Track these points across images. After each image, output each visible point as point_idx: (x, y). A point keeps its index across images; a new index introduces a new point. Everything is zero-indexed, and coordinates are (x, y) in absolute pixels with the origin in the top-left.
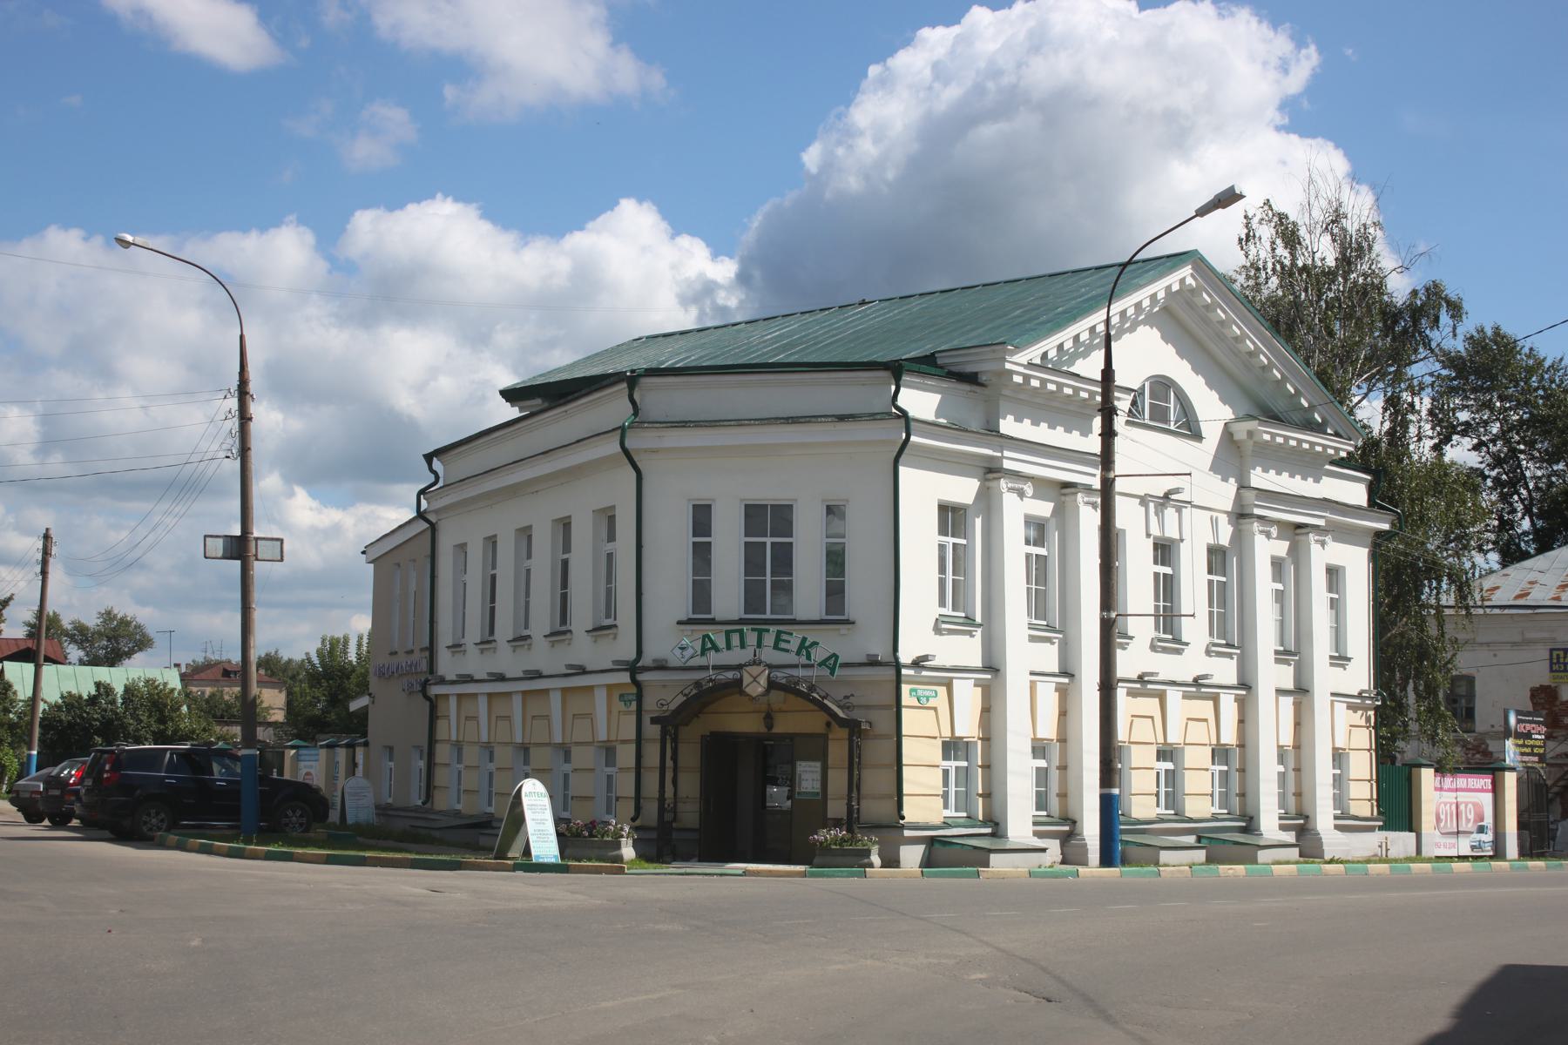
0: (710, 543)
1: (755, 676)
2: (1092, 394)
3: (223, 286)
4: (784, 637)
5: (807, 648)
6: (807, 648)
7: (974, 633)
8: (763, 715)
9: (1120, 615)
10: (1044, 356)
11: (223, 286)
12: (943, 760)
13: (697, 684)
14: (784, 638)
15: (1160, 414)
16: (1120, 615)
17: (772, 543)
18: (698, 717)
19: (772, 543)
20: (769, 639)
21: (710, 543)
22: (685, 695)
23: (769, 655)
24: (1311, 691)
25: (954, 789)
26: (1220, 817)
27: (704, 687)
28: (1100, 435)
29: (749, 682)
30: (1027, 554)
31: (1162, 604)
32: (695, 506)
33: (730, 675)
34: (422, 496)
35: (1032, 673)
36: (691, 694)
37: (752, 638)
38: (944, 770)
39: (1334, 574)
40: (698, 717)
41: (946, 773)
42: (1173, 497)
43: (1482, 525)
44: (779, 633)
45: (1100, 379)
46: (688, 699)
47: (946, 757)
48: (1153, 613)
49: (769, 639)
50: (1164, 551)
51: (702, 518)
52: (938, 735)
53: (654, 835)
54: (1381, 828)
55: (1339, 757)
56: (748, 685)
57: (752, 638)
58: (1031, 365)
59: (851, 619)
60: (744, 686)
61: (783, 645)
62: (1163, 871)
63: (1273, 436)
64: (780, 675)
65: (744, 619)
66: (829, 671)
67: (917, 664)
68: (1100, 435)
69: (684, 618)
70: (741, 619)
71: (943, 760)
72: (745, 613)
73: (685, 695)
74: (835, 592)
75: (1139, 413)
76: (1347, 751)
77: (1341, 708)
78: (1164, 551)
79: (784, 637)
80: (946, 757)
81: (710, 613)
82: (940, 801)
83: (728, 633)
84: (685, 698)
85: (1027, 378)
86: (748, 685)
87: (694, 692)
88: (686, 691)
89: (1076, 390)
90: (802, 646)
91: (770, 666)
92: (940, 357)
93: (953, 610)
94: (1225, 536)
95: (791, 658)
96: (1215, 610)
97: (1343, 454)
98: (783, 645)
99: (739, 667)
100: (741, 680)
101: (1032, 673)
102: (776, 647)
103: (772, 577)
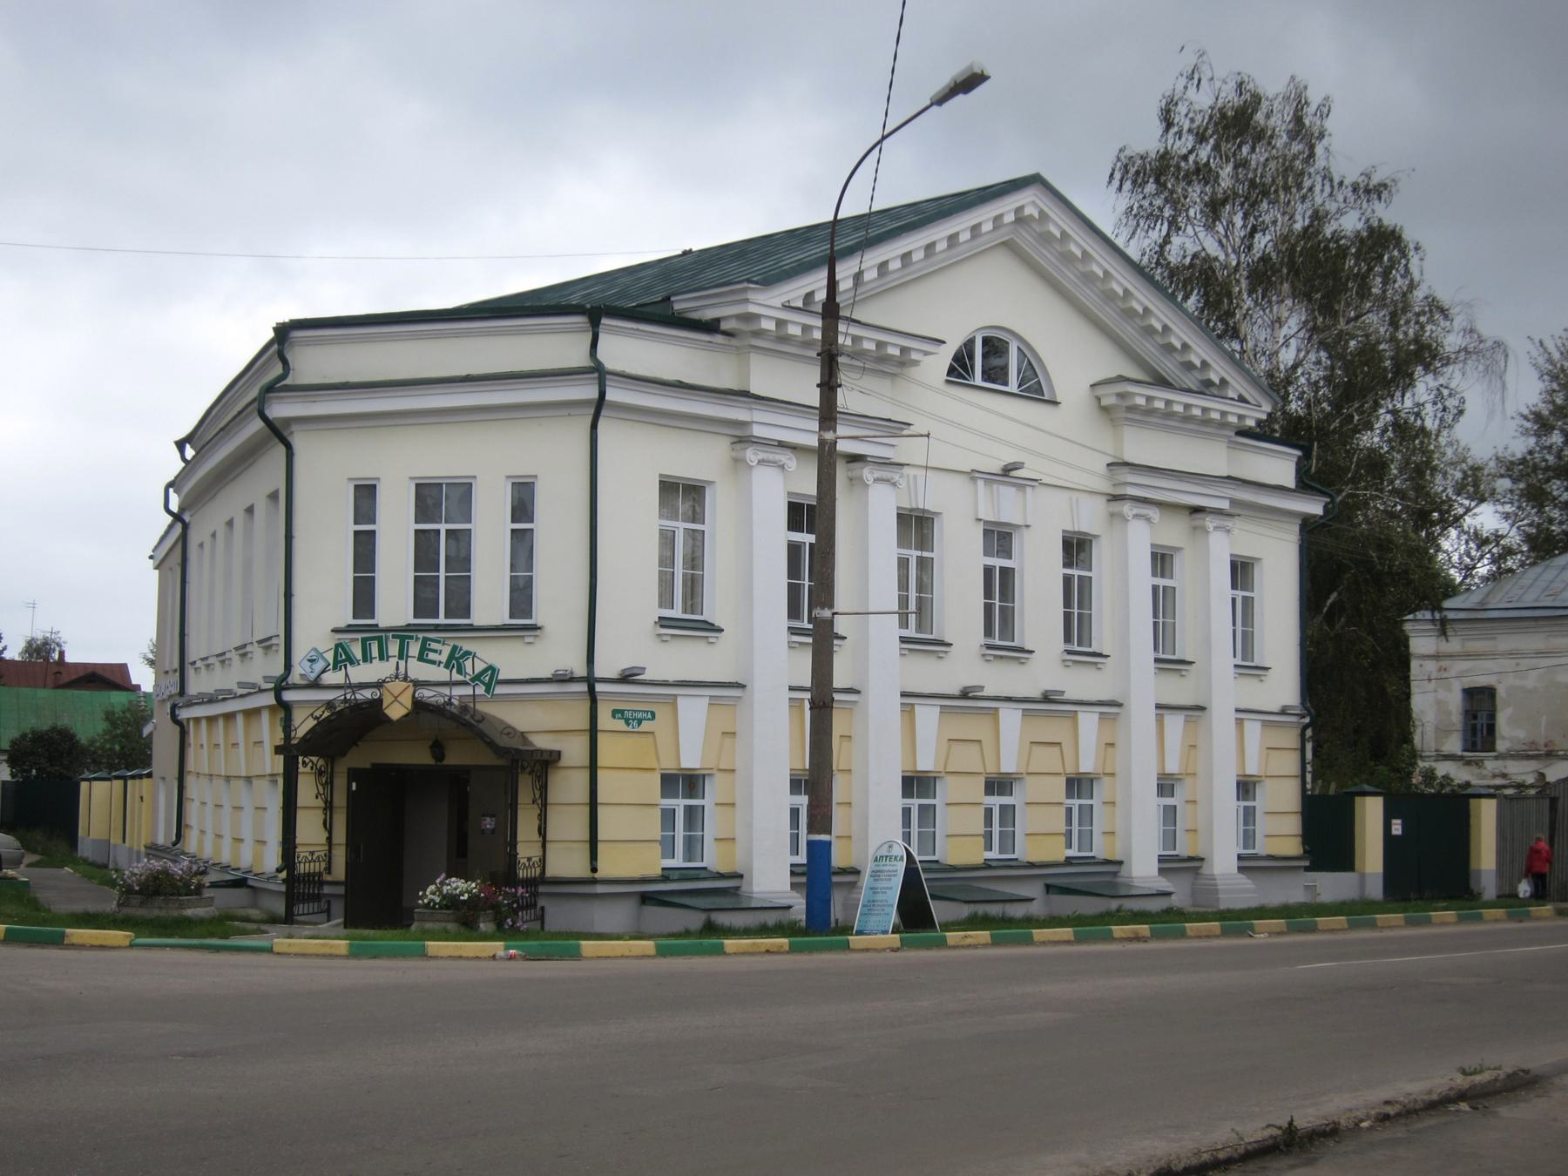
0: (374, 532)
1: (396, 695)
2: (806, 329)
3: (1051, 434)
4: (434, 646)
5: (457, 659)
6: (457, 659)
7: (1184, 673)
8: (430, 743)
9: (837, 613)
10: (809, 297)
11: (1051, 434)
12: (663, 797)
13: (329, 704)
14: (431, 647)
15: (996, 374)
16: (837, 613)
17: (447, 531)
18: (357, 746)
19: (447, 531)
20: (414, 649)
21: (374, 532)
22: (316, 718)
23: (418, 670)
24: (1208, 708)
25: (1077, 828)
26: (994, 864)
27: (338, 709)
28: (818, 386)
29: (390, 701)
30: (1153, 585)
31: (1161, 620)
32: (357, 487)
33: (367, 694)
34: (171, 490)
35: (1238, 710)
36: (323, 717)
37: (393, 648)
38: (1067, 808)
39: (1241, 571)
40: (357, 746)
41: (1069, 811)
42: (1014, 473)
43: (1553, 528)
44: (425, 640)
45: (820, 311)
46: (319, 723)
47: (1069, 795)
48: (896, 609)
49: (414, 649)
50: (999, 538)
51: (366, 495)
52: (1062, 771)
53: (803, 879)
54: (1307, 869)
55: (1246, 788)
56: (387, 707)
57: (393, 648)
58: (787, 307)
59: (539, 624)
60: (384, 706)
61: (432, 656)
62: (852, 940)
63: (1149, 399)
64: (426, 694)
65: (414, 625)
66: (484, 688)
67: (626, 678)
68: (818, 386)
69: (342, 624)
70: (409, 625)
71: (1067, 798)
72: (415, 617)
73: (316, 718)
74: (521, 596)
75: (970, 376)
76: (1024, 775)
77: (1253, 729)
78: (999, 538)
79: (434, 646)
80: (1069, 795)
81: (373, 617)
82: (1063, 839)
83: (364, 641)
84: (315, 722)
85: (781, 323)
86: (387, 707)
87: (327, 714)
88: (318, 714)
89: (881, 345)
90: (451, 656)
91: (418, 684)
92: (676, 301)
93: (1243, 660)
94: (808, 487)
95: (442, 674)
96: (1076, 611)
97: (1251, 423)
98: (432, 656)
99: (379, 685)
100: (380, 701)
101: (792, 689)
102: (421, 658)
103: (446, 572)
